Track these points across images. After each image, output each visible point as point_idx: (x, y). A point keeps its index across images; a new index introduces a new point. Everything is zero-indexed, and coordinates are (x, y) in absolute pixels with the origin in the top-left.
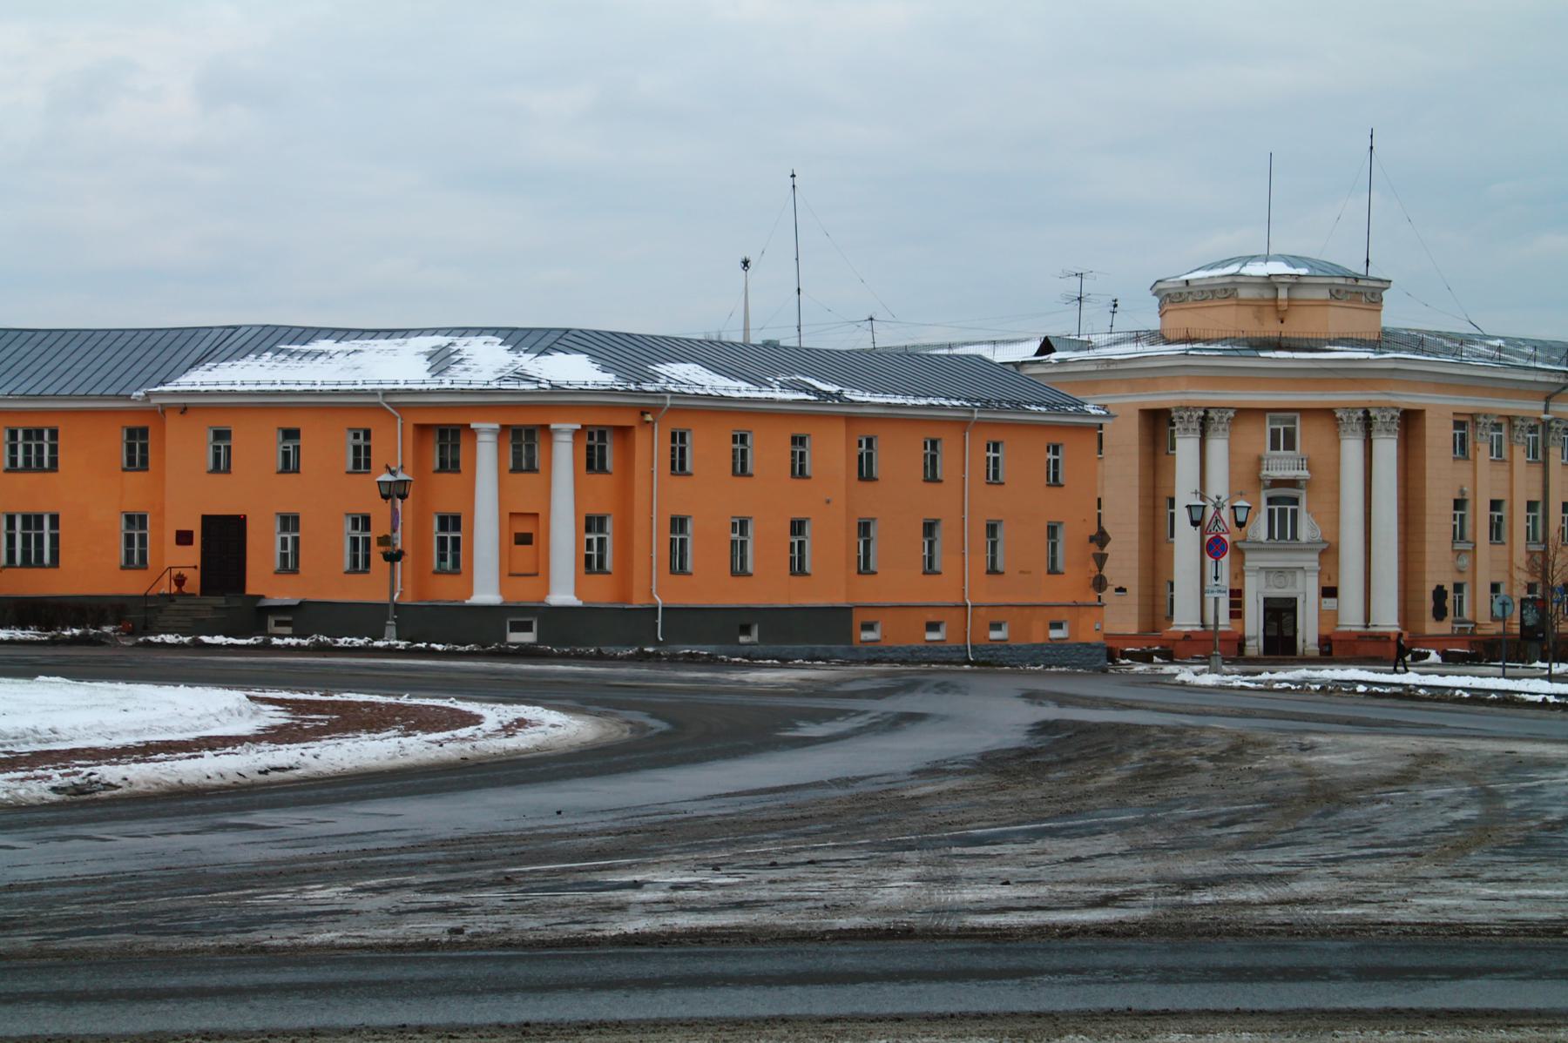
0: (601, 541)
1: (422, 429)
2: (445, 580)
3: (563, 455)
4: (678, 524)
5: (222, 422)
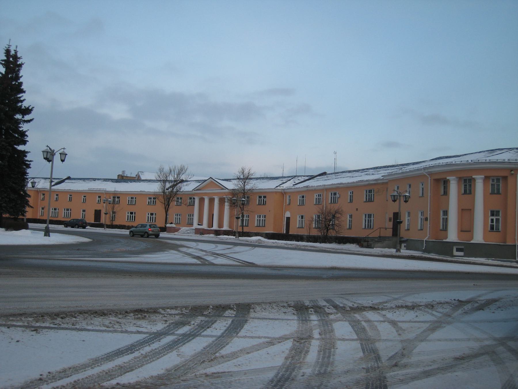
0: (497, 220)
1: (437, 181)
3: (479, 187)
5: (44, 193)
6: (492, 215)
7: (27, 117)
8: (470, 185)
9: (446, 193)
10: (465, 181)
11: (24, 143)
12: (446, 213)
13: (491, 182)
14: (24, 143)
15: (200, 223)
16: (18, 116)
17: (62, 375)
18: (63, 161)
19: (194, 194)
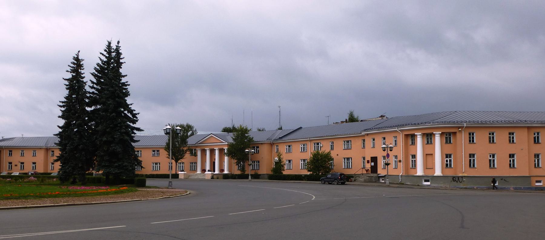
0: (450, 160)
1: (407, 136)
2: (413, 170)
3: (437, 140)
4: (472, 155)
6: (447, 157)
8: (431, 138)
9: (414, 143)
10: (412, 137)
12: (414, 156)
15: (213, 169)
19: (197, 147)
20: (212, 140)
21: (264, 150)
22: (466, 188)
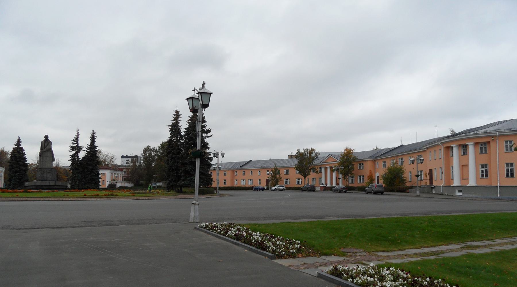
3: (471, 150)
7: (209, 134)
10: (463, 147)
11: (208, 148)
13: (480, 146)
14: (208, 148)
16: (205, 135)
17: (44, 187)
18: (223, 157)
19: (321, 165)
20: (331, 160)
21: (368, 166)
22: (491, 199)
